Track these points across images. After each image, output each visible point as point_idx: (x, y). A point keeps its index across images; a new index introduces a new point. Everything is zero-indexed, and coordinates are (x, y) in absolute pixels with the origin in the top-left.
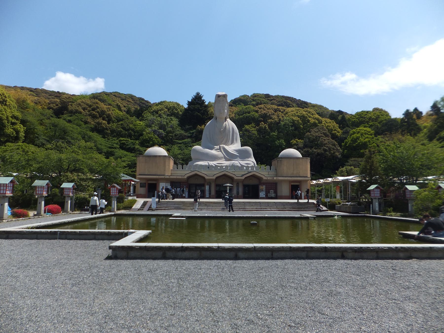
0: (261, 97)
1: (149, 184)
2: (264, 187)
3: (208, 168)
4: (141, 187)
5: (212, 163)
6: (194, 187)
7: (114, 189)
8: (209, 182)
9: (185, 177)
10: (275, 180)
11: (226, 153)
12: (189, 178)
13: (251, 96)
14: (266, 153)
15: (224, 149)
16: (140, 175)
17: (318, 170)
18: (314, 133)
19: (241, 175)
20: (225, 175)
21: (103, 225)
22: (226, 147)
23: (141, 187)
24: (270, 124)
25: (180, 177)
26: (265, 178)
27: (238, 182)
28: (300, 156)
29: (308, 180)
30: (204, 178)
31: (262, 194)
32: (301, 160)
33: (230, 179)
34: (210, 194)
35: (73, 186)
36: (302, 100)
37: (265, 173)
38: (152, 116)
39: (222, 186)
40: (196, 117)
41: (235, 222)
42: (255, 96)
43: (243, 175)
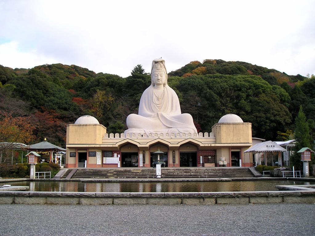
3: (142, 136)
4: (70, 156)
6: (129, 154)
7: (32, 156)
8: (144, 149)
11: (161, 120)
19: (177, 143)
23: (70, 156)
24: (210, 89)
25: (111, 146)
26: (201, 145)
27: (174, 149)
28: (241, 121)
30: (166, 146)
32: (241, 126)
34: (144, 163)
37: (203, 140)
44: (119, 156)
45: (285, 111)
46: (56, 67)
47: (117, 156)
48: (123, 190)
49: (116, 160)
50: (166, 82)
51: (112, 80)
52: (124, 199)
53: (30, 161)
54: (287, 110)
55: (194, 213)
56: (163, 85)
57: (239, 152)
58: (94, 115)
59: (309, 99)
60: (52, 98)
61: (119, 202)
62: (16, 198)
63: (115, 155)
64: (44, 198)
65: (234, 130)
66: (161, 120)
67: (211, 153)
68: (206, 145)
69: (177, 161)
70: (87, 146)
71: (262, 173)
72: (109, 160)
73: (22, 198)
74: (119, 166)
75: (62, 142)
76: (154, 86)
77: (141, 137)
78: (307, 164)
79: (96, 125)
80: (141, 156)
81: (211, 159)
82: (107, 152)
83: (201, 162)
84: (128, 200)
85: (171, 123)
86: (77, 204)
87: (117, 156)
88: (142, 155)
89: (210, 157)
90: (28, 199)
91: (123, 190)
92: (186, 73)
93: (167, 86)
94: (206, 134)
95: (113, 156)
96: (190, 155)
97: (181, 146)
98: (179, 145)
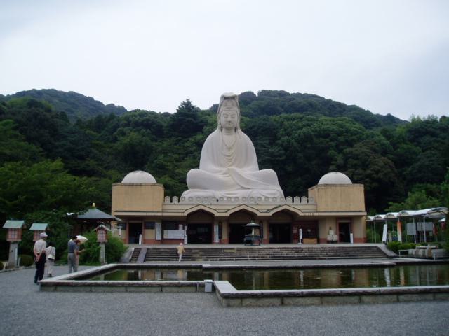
0: (275, 97)
1: (130, 224)
2: (207, 230)
3: (217, 200)
5: (219, 194)
7: (101, 232)
8: (221, 220)
9: (186, 214)
10: (316, 216)
11: (232, 177)
12: (190, 215)
13: (260, 93)
14: (297, 179)
15: (237, 173)
16: (117, 211)
17: (375, 202)
18: (359, 148)
19: (183, 211)
20: (243, 211)
21: (158, 275)
22: (239, 171)
24: (296, 135)
25: (178, 214)
26: (301, 214)
27: (261, 220)
28: (350, 182)
29: (362, 216)
30: (211, 215)
31: (216, 239)
32: (351, 188)
33: (251, 216)
35: (23, 226)
36: (333, 100)
37: (301, 207)
38: (277, 119)
39: (240, 226)
40: (189, 126)
41: (411, 269)
42: (266, 95)
43: (228, 210)
44: (186, 228)
45: (391, 167)
46: (48, 94)
47: (184, 229)
48: (190, 277)
49: (181, 233)
50: (238, 125)
51: (147, 117)
52: (410, 296)
53: (99, 239)
54: (392, 164)
55: (351, 312)
56: (233, 130)
57: (348, 223)
58: (340, 169)
59: (111, 147)
60: (64, 142)
61: (405, 299)
62: (285, 299)
63: (181, 226)
64: (319, 298)
65: (337, 193)
66: (232, 177)
67: (312, 226)
68: (307, 214)
69: (225, 236)
70: (144, 214)
71: (397, 253)
72: (170, 234)
73: (293, 299)
74: (186, 241)
75: (106, 207)
76: (222, 130)
77: (215, 203)
78: (16, 245)
79: (348, 185)
80: (216, 229)
81: (311, 232)
82: (170, 223)
83: (301, 237)
84: (414, 296)
85: (248, 182)
86: (279, 305)
87: (184, 229)
88: (218, 227)
89: (309, 230)
90: (300, 299)
91: (189, 278)
92: (273, 114)
93: (239, 130)
94: (304, 198)
95: (177, 228)
96: (283, 227)
97: (231, 214)
98: (228, 214)
